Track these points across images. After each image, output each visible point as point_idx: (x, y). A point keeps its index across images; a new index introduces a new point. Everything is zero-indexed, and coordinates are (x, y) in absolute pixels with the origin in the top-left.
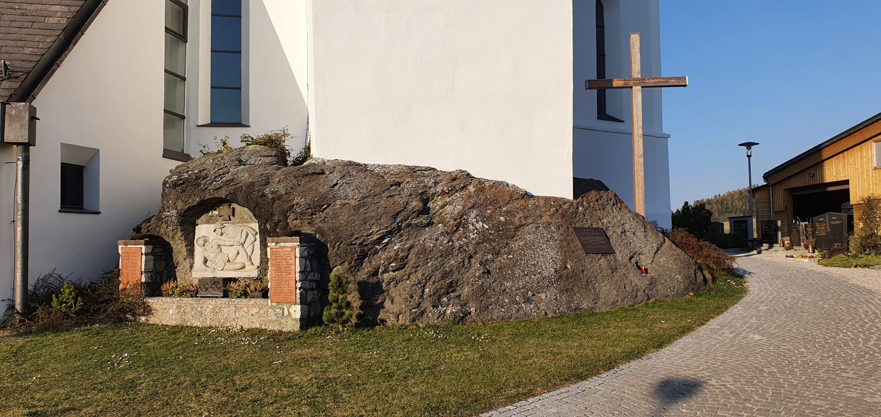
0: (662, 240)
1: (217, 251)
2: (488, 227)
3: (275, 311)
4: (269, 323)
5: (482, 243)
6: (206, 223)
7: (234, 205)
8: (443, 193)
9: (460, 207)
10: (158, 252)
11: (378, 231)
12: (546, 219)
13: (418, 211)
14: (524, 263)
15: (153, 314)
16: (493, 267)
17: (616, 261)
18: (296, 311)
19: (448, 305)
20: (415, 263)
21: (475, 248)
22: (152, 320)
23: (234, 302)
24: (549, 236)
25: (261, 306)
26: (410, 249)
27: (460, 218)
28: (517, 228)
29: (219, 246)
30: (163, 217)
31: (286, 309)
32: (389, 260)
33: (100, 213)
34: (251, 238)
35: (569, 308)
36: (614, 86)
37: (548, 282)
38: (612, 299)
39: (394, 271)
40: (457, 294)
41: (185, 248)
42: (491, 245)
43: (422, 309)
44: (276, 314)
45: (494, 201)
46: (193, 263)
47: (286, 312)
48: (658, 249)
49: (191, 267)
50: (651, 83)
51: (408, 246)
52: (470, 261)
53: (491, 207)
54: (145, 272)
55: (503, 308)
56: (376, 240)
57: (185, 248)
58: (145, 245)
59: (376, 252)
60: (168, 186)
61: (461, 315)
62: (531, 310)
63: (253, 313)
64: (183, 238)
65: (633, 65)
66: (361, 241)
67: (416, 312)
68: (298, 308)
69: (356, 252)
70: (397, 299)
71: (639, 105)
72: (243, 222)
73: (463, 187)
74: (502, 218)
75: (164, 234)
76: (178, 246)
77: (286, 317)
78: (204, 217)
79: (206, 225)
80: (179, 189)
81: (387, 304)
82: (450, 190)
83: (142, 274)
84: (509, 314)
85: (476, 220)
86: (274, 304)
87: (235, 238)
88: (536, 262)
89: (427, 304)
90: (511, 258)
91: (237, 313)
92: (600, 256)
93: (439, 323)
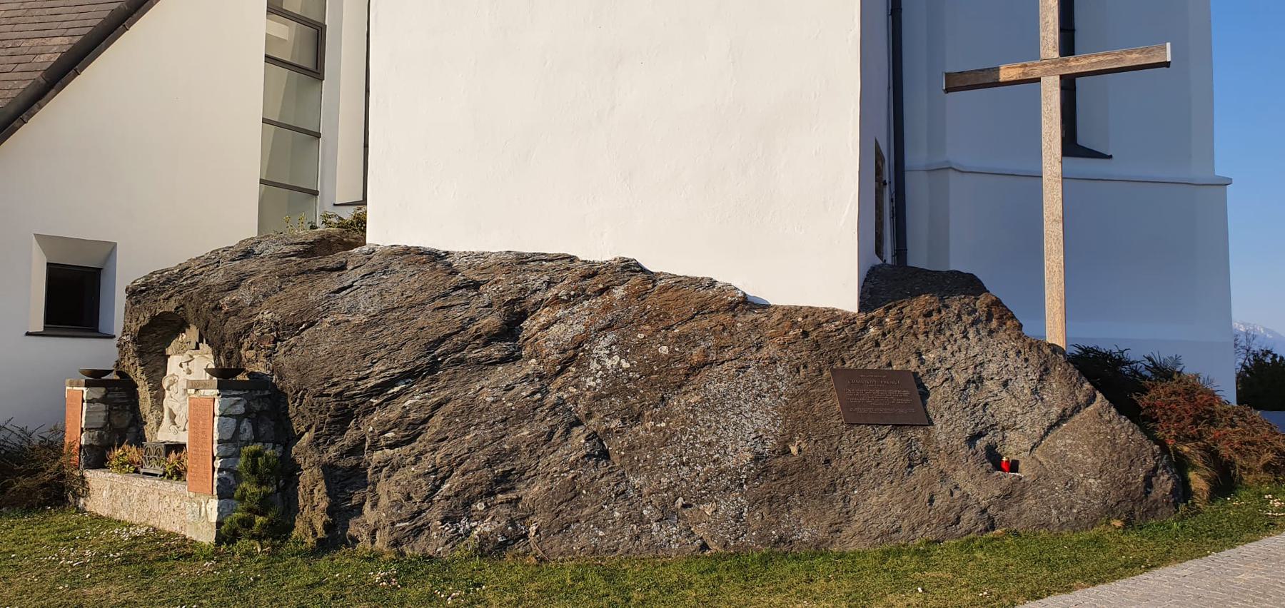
0: (1081, 398)
1: (183, 398)
2: (628, 366)
5: (608, 396)
8: (557, 300)
9: (581, 328)
10: (115, 398)
11: (381, 372)
12: (770, 350)
13: (486, 334)
14: (687, 439)
16: (615, 446)
17: (928, 441)
19: (483, 518)
20: (438, 433)
21: (588, 407)
24: (765, 386)
26: (439, 405)
27: (575, 348)
28: (694, 369)
32: (384, 427)
35: (762, 538)
36: (1001, 79)
37: (731, 480)
38: (884, 523)
39: (391, 447)
40: (511, 495)
41: (148, 393)
42: (626, 401)
43: (420, 523)
45: (658, 315)
48: (1063, 418)
50: (1083, 66)
51: (436, 399)
52: (568, 431)
53: (647, 327)
54: (86, 429)
55: (604, 529)
56: (372, 387)
57: (148, 393)
58: (86, 386)
59: (369, 411)
61: (500, 540)
62: (670, 536)
65: (1042, 34)
66: (341, 389)
67: (404, 529)
68: (214, 503)
69: (328, 409)
70: (384, 501)
73: (601, 289)
74: (665, 348)
78: (175, 344)
82: (573, 296)
84: (611, 543)
85: (608, 352)
88: (714, 439)
89: (434, 515)
90: (661, 429)
92: (886, 431)
93: (445, 553)
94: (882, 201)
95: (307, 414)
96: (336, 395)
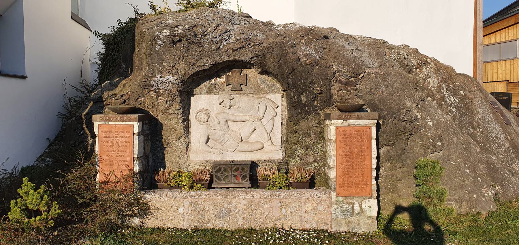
3: (341, 207)
4: (331, 222)
6: (207, 93)
15: (152, 214)
22: (151, 222)
23: (279, 195)
25: (319, 201)
30: (154, 83)
31: (357, 204)
33: (27, 77)
34: (270, 112)
44: (343, 212)
46: (189, 143)
47: (357, 209)
60: (161, 42)
63: (309, 209)
71: (481, 3)
72: (258, 93)
75: (150, 107)
77: (357, 214)
79: (206, 95)
80: (181, 47)
83: (134, 161)
86: (340, 199)
87: (248, 112)
91: (284, 210)
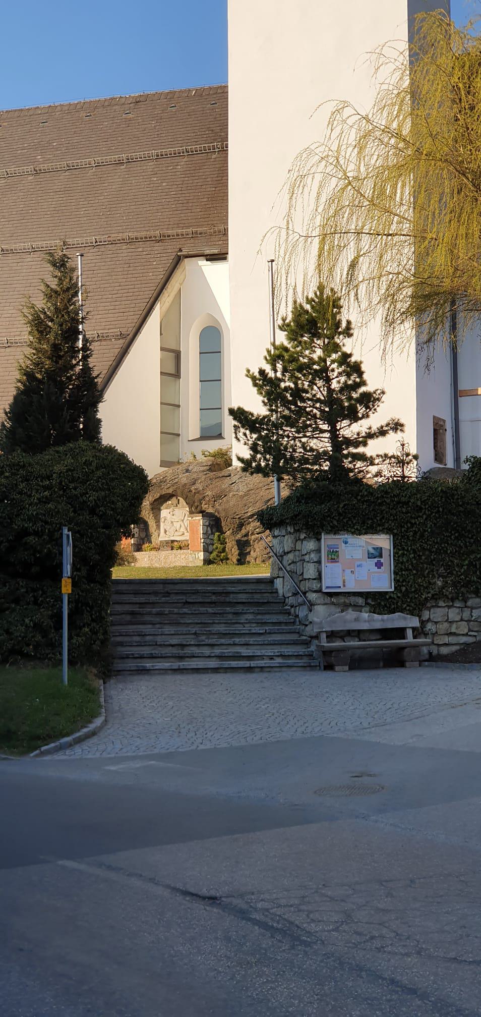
7: (179, 498)
18: (201, 555)
22: (138, 565)
29: (172, 522)
39: (258, 534)
47: (197, 557)
49: (159, 535)
59: (249, 523)
64: (153, 518)
68: (202, 553)
70: (257, 550)
76: (152, 523)
78: (164, 505)
81: (252, 553)
94: (443, 441)
95: (229, 525)
96: (238, 518)
